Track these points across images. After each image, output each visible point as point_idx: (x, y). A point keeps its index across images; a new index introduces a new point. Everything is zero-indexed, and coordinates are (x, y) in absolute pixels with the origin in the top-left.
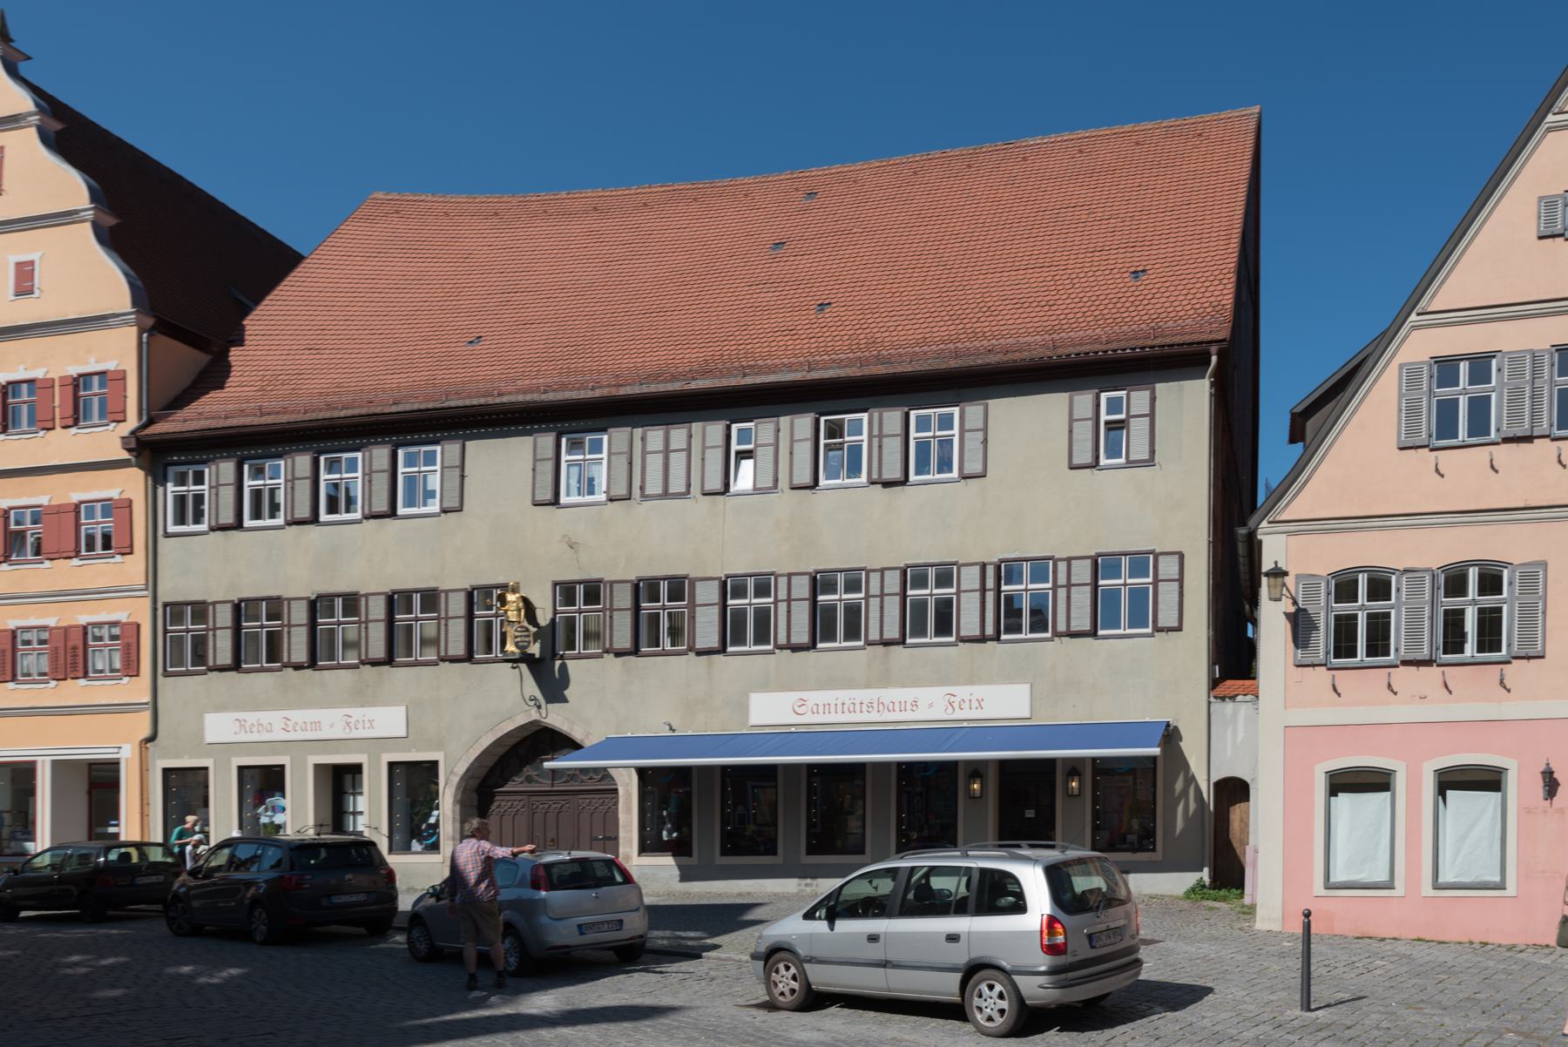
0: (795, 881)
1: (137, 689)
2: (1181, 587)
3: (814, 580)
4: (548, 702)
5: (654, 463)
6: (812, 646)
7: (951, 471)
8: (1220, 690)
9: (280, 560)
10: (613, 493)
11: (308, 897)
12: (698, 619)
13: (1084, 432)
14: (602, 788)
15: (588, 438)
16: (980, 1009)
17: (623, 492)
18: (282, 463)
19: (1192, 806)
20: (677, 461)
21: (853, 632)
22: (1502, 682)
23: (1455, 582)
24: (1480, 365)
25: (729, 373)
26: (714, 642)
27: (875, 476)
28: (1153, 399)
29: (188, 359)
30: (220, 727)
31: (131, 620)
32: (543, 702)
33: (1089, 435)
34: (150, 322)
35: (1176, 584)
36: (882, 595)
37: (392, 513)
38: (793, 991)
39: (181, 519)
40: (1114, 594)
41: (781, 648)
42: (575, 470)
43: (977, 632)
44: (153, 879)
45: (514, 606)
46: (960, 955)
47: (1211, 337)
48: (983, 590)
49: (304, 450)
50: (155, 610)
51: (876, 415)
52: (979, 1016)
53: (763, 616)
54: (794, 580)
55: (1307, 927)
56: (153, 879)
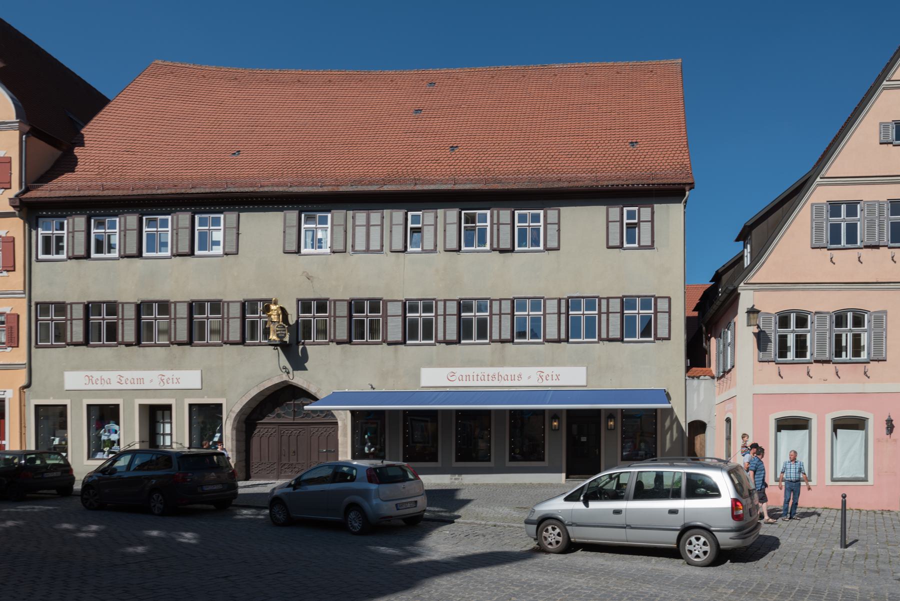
0: (449, 476)
1: (19, 355)
2: (670, 316)
3: (459, 304)
4: (294, 370)
5: (361, 232)
6: (458, 342)
7: (539, 246)
8: (690, 373)
9: (115, 278)
10: (335, 249)
11: (169, 485)
12: (389, 324)
13: (615, 228)
14: (329, 421)
15: (318, 215)
16: (691, 552)
17: (342, 248)
18: (117, 219)
19: (675, 435)
20: (375, 232)
21: (482, 334)
22: (865, 373)
23: (840, 319)
24: (852, 207)
25: (405, 182)
26: (399, 338)
27: (495, 246)
28: (653, 213)
29: (47, 153)
30: (74, 380)
31: (13, 312)
32: (291, 369)
33: (618, 230)
34: (27, 128)
35: (667, 315)
36: (500, 314)
37: (139, 255)
38: (557, 542)
39: (47, 251)
40: (577, 319)
41: (440, 342)
42: (310, 233)
43: (556, 337)
44: (55, 474)
45: (275, 313)
46: (678, 522)
47: (684, 181)
48: (559, 313)
49: (186, 211)
50: (30, 306)
51: (495, 212)
52: (690, 556)
53: (428, 324)
54: (448, 303)
55: (844, 503)
56: (55, 474)
